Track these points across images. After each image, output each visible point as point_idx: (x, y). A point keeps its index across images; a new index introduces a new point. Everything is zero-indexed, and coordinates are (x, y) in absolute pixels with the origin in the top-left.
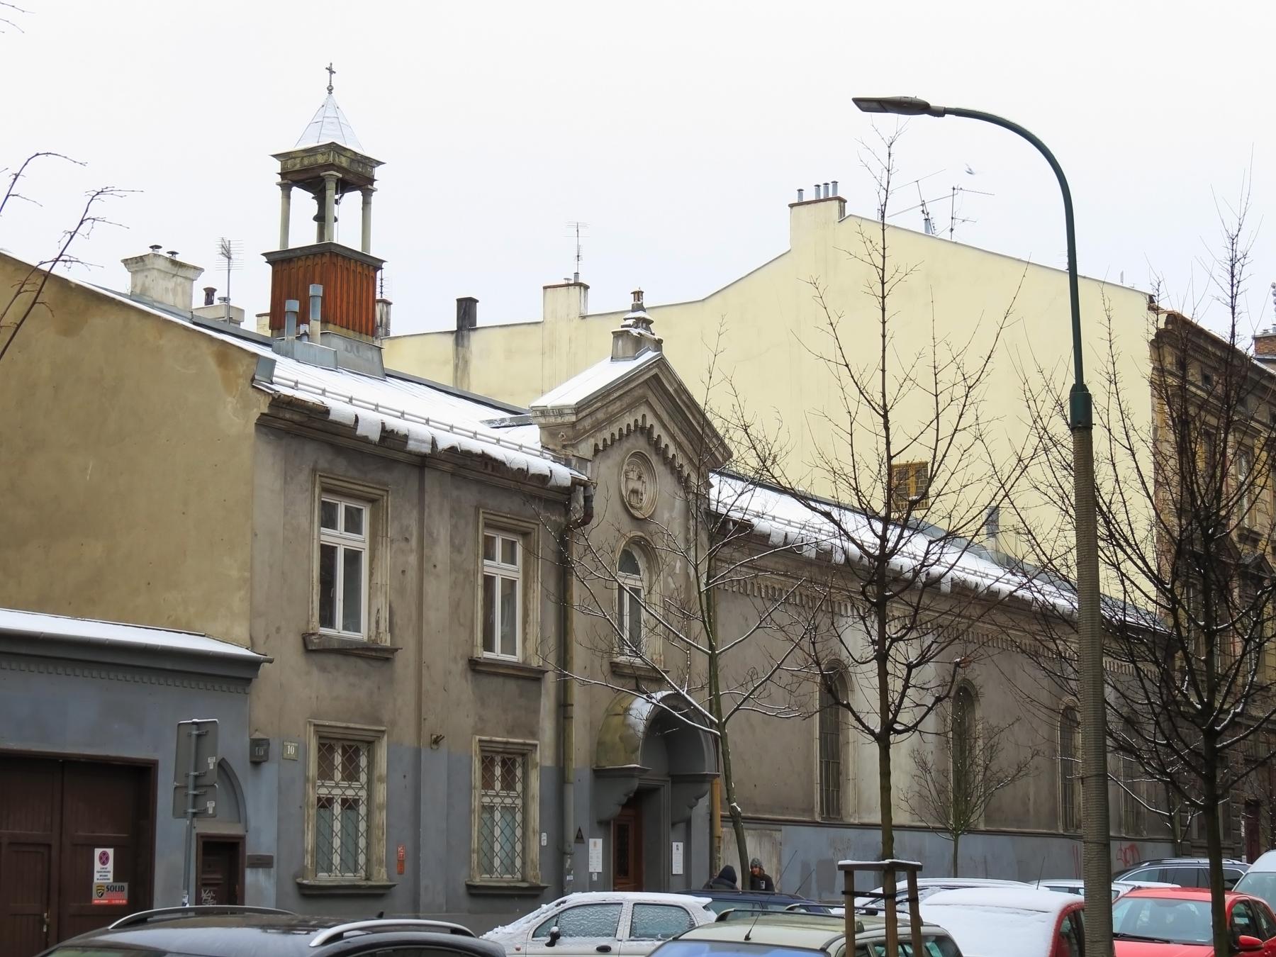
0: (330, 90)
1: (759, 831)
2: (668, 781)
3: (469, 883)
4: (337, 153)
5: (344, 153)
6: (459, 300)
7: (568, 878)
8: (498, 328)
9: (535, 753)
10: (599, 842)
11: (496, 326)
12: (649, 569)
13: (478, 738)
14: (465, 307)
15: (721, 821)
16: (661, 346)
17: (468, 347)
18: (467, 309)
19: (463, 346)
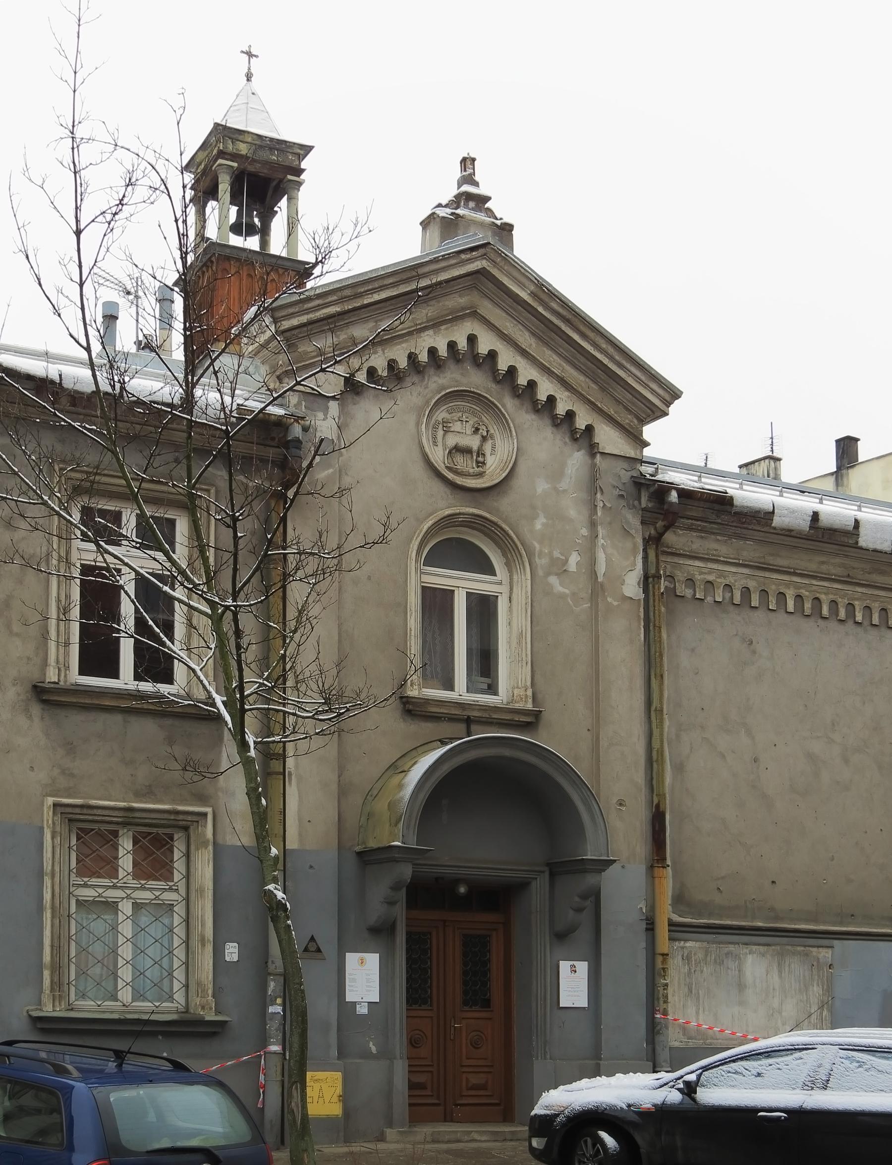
0: (249, 77)
1: (778, 948)
2: (543, 872)
3: (35, 1014)
4: (230, 138)
5: (241, 138)
6: (838, 442)
7: (271, 1009)
8: (875, 462)
9: (205, 826)
10: (373, 960)
11: (873, 459)
12: (508, 565)
13: (50, 800)
14: (844, 446)
15: (669, 931)
16: (512, 234)
17: (847, 486)
18: (845, 448)
19: (842, 485)
